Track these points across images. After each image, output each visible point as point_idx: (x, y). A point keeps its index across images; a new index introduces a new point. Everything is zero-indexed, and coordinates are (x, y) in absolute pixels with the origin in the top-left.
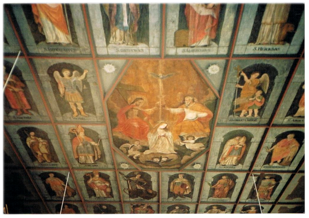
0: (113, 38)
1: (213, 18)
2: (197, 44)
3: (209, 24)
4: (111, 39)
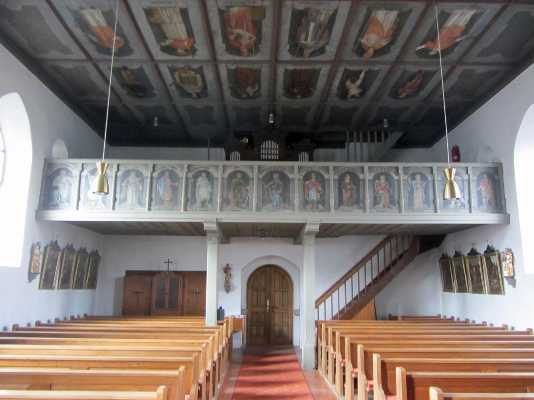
0: (329, 14)
1: (230, 27)
2: (240, 9)
3: (233, 23)
4: (331, 13)
